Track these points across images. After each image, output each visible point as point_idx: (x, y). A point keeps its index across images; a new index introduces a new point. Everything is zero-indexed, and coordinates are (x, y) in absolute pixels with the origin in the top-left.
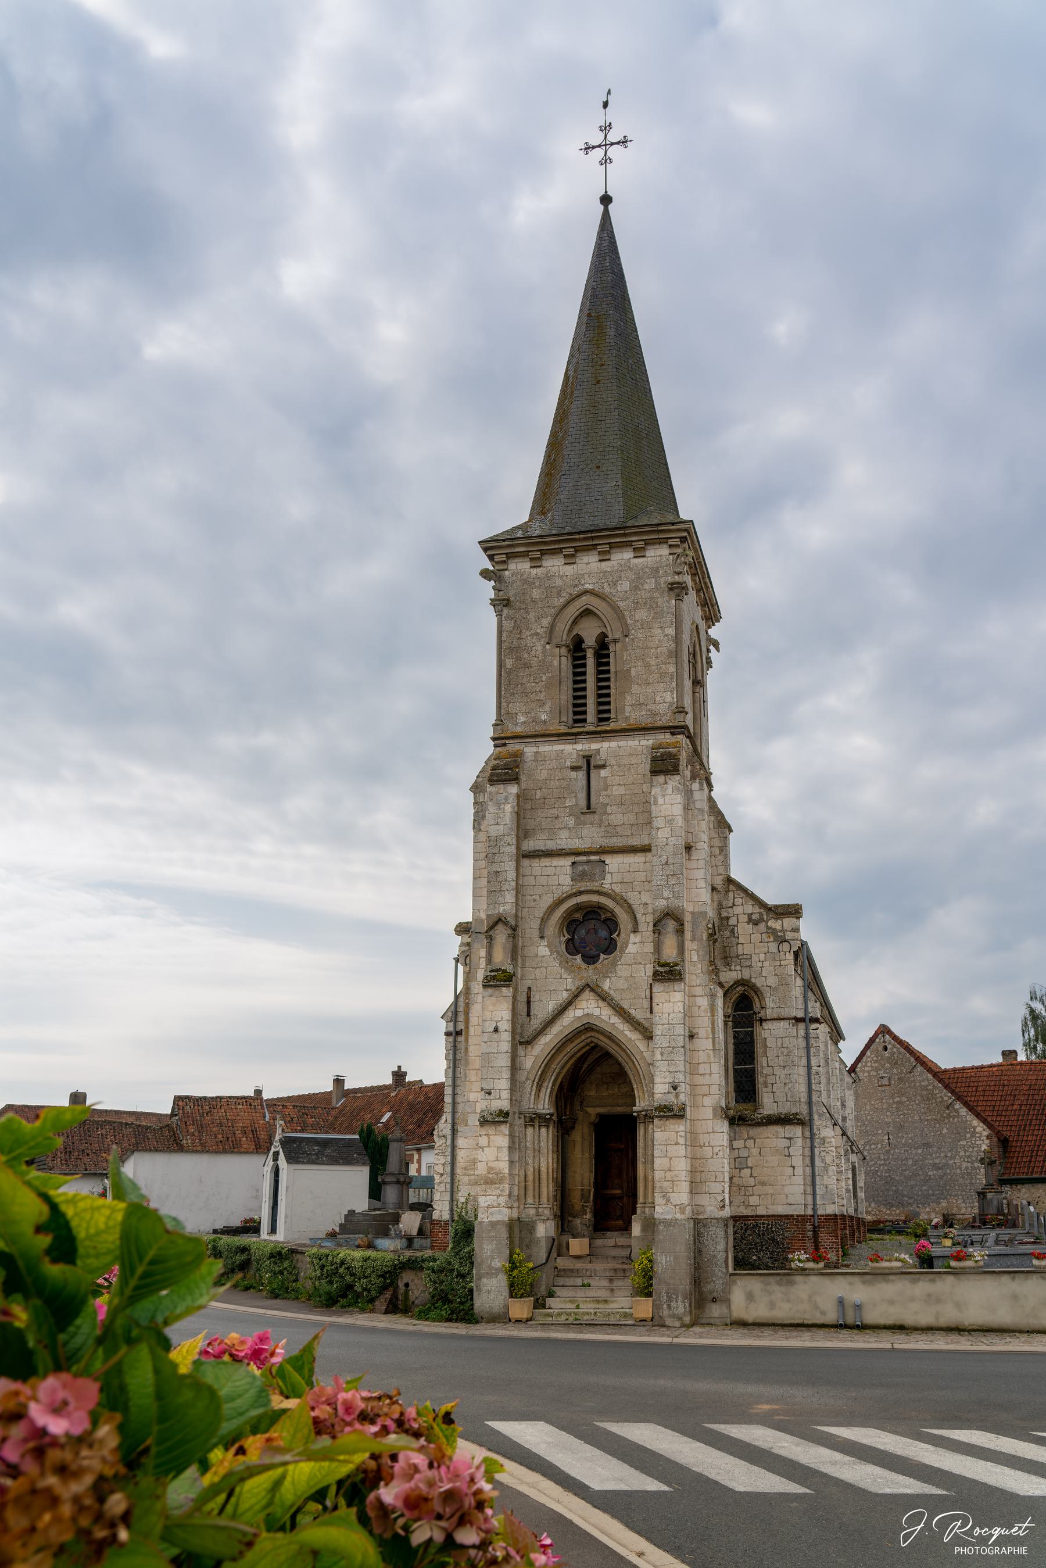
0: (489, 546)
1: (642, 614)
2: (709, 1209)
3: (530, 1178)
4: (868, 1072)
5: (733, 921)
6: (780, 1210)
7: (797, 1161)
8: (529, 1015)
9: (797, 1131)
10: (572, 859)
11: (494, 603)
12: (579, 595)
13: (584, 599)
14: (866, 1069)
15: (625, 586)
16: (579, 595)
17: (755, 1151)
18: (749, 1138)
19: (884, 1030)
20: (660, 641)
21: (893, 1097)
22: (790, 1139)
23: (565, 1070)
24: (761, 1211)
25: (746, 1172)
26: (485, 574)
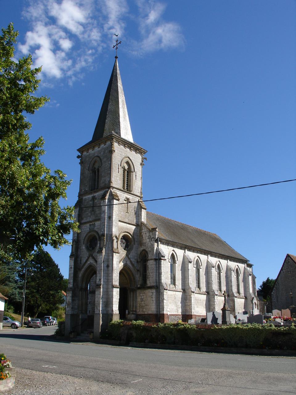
0: (79, 150)
1: (105, 159)
2: (110, 311)
3: (80, 304)
4: (285, 270)
5: (142, 234)
6: (150, 312)
7: (154, 299)
8: (81, 264)
9: (154, 291)
10: (89, 224)
11: (80, 163)
12: (94, 158)
13: (95, 158)
14: (285, 269)
15: (102, 153)
16: (94, 158)
17: (145, 296)
18: (144, 293)
19: (288, 256)
20: (108, 165)
21: (292, 278)
22: (152, 293)
23: (239, 271)
24: (146, 313)
25: (143, 302)
26: (78, 157)
